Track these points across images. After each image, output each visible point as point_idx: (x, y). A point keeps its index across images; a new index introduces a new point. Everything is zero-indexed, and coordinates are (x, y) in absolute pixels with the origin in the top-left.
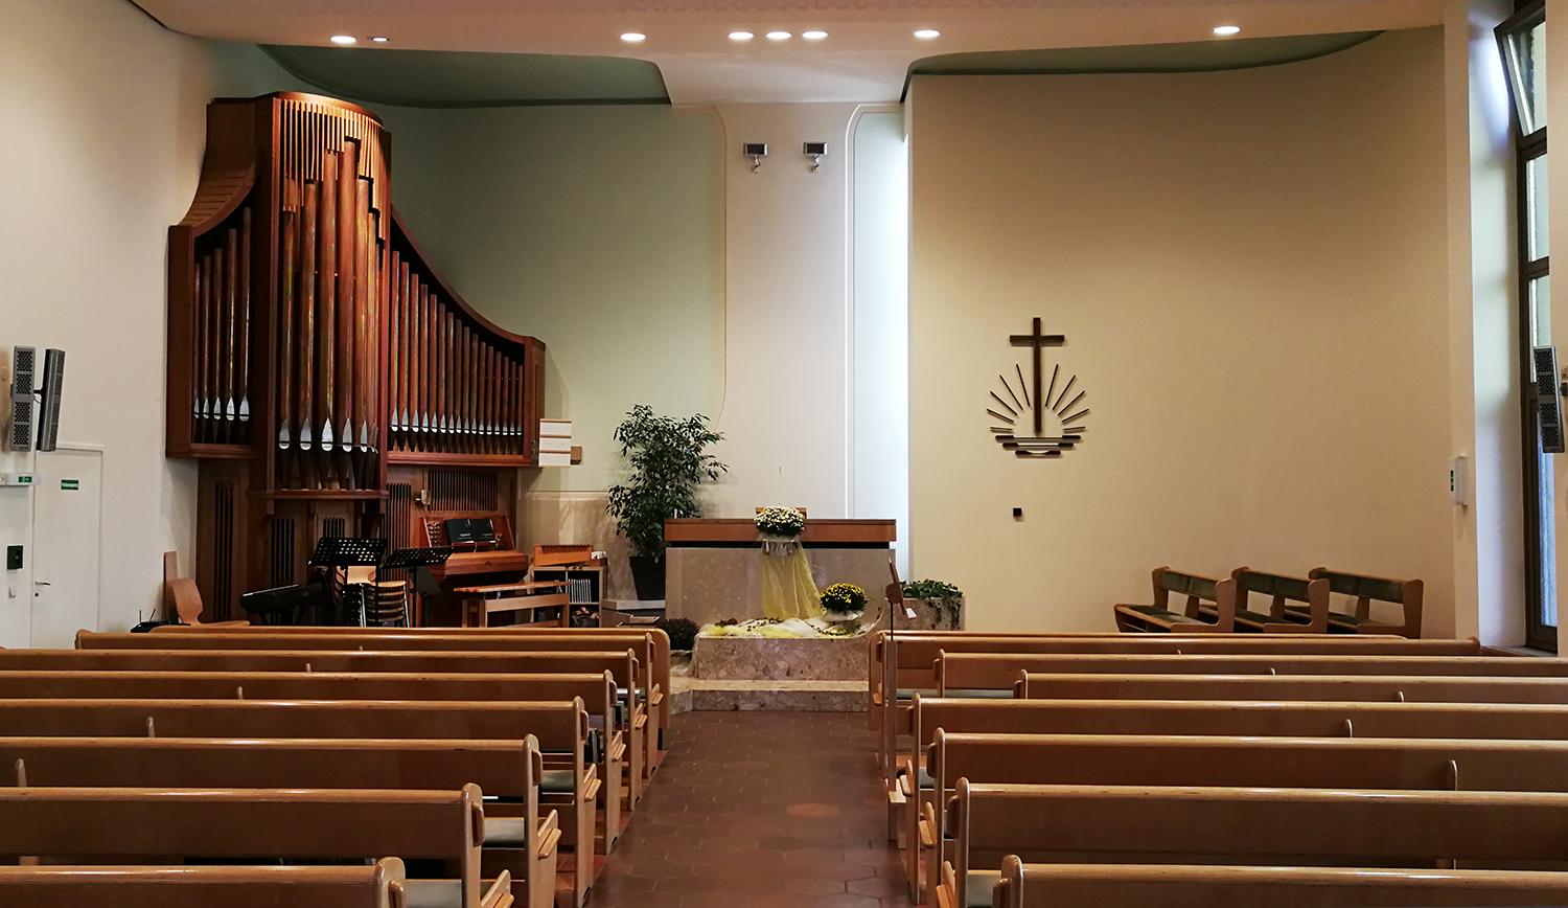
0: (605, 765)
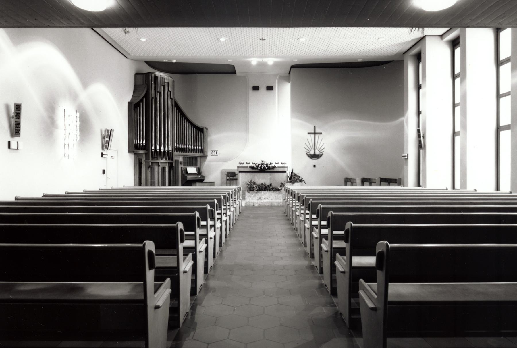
0: (178, 277)
